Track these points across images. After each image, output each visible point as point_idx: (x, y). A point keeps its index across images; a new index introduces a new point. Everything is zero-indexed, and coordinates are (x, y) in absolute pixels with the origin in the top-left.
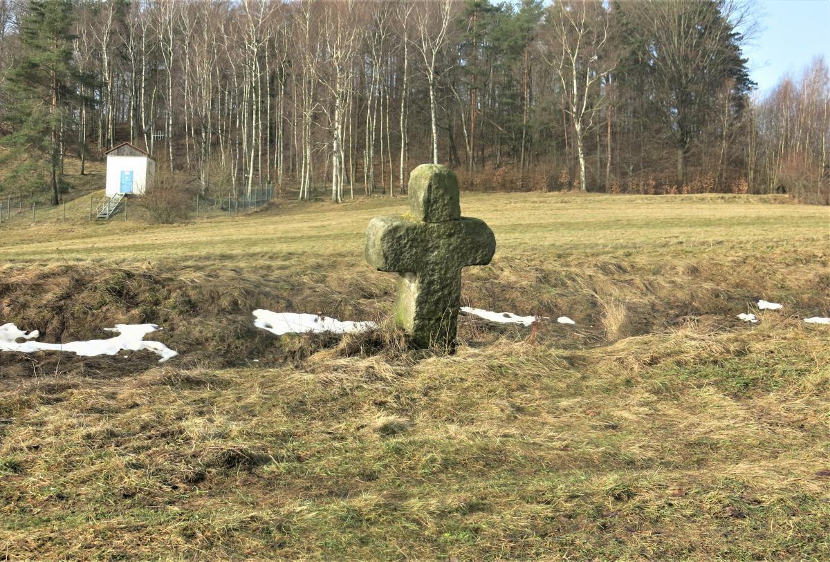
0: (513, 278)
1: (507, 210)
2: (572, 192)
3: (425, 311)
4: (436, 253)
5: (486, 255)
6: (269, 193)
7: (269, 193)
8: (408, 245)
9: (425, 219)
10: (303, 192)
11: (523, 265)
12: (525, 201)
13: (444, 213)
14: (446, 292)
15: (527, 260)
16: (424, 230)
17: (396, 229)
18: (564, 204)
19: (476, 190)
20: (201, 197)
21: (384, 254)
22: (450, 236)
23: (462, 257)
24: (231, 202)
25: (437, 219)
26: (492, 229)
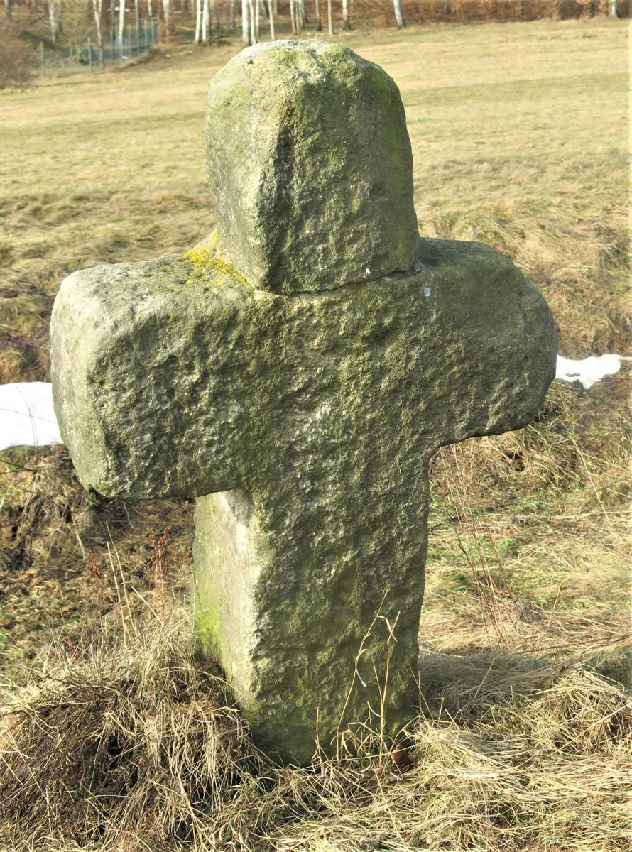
0: (548, 256)
1: (503, 53)
2: (596, 19)
3: (293, 624)
4: (325, 408)
5: (522, 397)
6: (149, 34)
7: (149, 34)
8: (206, 394)
9: (272, 281)
10: (201, 32)
11: (566, 219)
12: (529, 37)
13: (351, 252)
14: (372, 547)
15: (576, 206)
16: (272, 325)
17: (149, 332)
18: (587, 41)
19: (455, 21)
20: (48, 45)
21: (109, 438)
22: (380, 337)
23: (430, 413)
24: (93, 51)
25: (322, 280)
26: (556, 300)
